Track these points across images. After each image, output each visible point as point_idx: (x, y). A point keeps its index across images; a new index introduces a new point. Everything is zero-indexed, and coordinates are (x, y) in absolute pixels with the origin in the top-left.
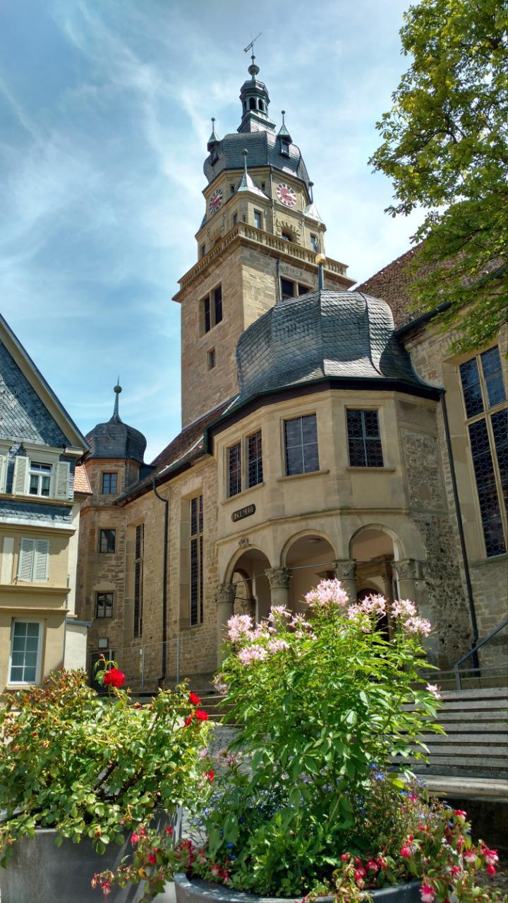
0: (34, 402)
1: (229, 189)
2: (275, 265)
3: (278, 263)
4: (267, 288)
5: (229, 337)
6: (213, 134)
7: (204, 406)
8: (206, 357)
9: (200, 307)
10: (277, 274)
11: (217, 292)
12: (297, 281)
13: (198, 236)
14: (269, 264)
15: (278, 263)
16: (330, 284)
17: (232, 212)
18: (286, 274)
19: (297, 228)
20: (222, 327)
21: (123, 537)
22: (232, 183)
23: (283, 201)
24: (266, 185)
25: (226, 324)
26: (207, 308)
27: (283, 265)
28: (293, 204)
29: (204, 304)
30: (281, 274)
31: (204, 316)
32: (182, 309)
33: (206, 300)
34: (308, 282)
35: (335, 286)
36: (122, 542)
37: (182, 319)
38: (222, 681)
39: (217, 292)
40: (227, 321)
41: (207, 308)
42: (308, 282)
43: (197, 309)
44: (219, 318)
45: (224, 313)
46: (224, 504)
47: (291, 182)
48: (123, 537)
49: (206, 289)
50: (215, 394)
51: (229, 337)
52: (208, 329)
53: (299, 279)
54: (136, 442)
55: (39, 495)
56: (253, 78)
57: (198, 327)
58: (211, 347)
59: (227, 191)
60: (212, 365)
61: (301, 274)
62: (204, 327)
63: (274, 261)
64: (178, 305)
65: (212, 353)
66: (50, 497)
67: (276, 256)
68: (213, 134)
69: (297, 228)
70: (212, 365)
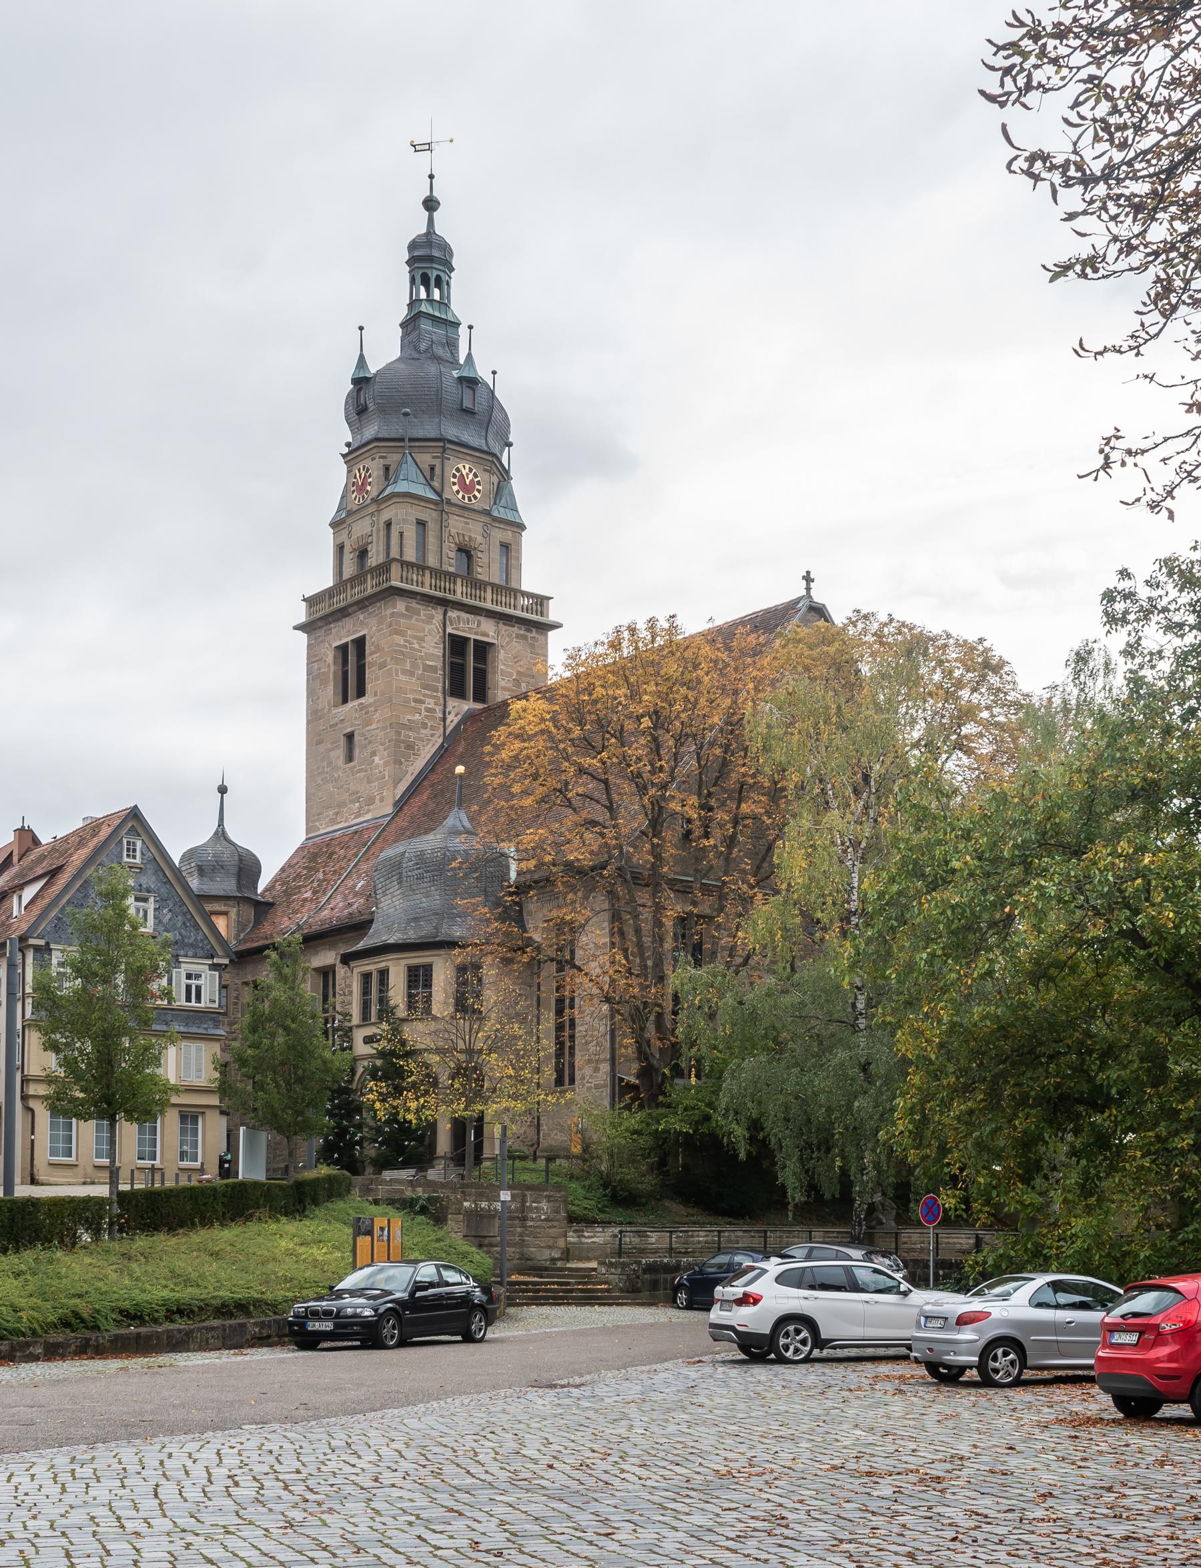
0: (184, 914)
1: (382, 473)
2: (441, 617)
3: (445, 614)
4: (429, 656)
5: (373, 726)
6: (362, 358)
7: (337, 814)
8: (342, 741)
9: (335, 658)
10: (444, 631)
11: (360, 643)
12: (473, 637)
13: (335, 525)
14: (432, 617)
15: (445, 614)
16: (522, 632)
17: (385, 516)
18: (457, 629)
19: (479, 539)
20: (362, 707)
21: (237, 998)
22: (387, 462)
23: (460, 496)
24: (438, 471)
25: (370, 705)
26: (345, 662)
27: (453, 614)
28: (475, 497)
29: (340, 655)
30: (449, 630)
31: (340, 673)
32: (309, 646)
33: (343, 649)
34: (488, 636)
35: (530, 635)
36: (236, 1004)
37: (308, 664)
38: (1138, 753)
39: (360, 643)
40: (371, 700)
41: (345, 662)
42: (488, 636)
43: (330, 659)
44: (361, 692)
45: (368, 687)
46: (358, 1026)
47: (475, 460)
48: (237, 998)
49: (344, 633)
50: (352, 802)
51: (373, 726)
52: (345, 701)
53: (476, 634)
54: (247, 867)
55: (193, 1003)
56: (431, 222)
57: (330, 691)
58: (349, 730)
59: (378, 476)
60: (350, 758)
61: (479, 625)
62: (340, 698)
63: (440, 610)
64: (303, 637)
65: (350, 737)
66: (202, 1005)
67: (444, 603)
68: (362, 358)
69: (479, 539)
70: (350, 758)
